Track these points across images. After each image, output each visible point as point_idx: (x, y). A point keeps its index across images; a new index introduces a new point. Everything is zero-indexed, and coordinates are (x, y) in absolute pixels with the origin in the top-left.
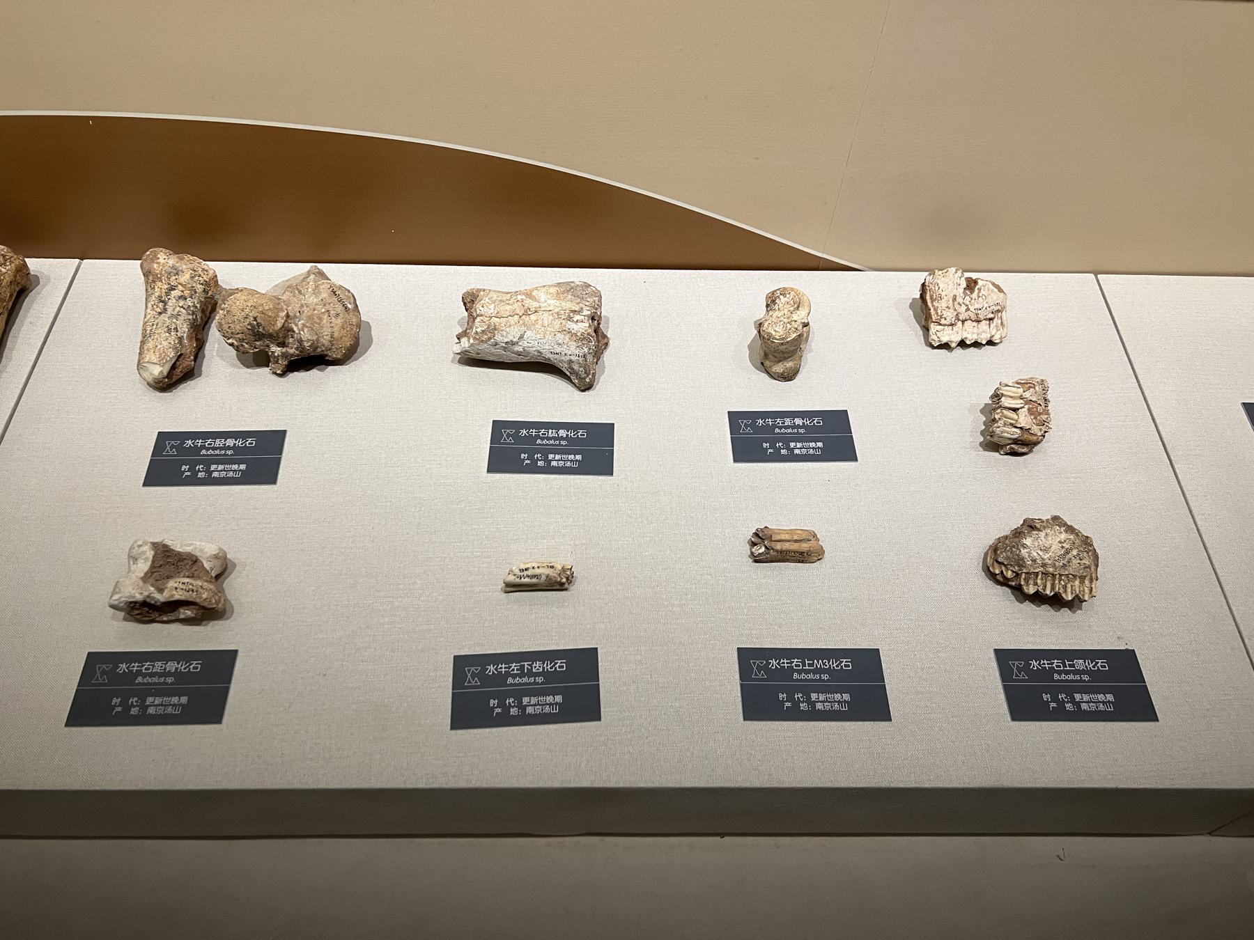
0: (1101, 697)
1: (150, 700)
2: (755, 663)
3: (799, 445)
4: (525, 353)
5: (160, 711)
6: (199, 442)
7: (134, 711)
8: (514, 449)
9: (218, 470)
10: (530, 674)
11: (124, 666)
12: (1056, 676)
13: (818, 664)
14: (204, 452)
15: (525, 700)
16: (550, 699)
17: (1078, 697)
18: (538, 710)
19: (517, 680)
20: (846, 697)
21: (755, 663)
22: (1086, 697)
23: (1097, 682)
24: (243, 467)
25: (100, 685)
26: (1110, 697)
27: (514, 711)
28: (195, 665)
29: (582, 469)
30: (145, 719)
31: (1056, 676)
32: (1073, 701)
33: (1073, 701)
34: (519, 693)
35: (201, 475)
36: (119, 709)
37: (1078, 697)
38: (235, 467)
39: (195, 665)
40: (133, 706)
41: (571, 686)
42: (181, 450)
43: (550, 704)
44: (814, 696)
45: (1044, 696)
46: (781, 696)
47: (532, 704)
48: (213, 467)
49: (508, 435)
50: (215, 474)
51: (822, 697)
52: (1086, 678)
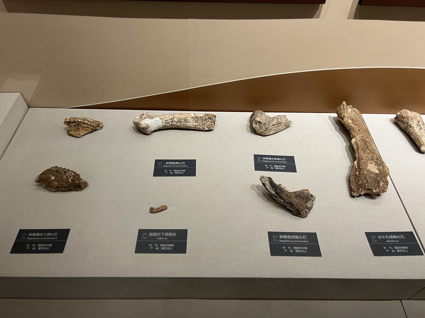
0: (403, 247)
1: (39, 245)
4: (187, 126)
7: (34, 249)
10: (164, 237)
11: (167, 233)
12: (387, 241)
15: (161, 245)
16: (170, 245)
17: (395, 248)
18: (165, 248)
19: (160, 239)
20: (306, 248)
23: (401, 243)
25: (23, 240)
26: (406, 248)
27: (157, 248)
28: (56, 234)
29: (185, 175)
31: (387, 241)
32: (394, 249)
34: (159, 243)
36: (29, 248)
37: (395, 248)
39: (175, 234)
40: (33, 247)
41: (177, 241)
43: (170, 247)
45: (283, 247)
46: (283, 247)
47: (163, 246)
51: (297, 248)
52: (397, 241)
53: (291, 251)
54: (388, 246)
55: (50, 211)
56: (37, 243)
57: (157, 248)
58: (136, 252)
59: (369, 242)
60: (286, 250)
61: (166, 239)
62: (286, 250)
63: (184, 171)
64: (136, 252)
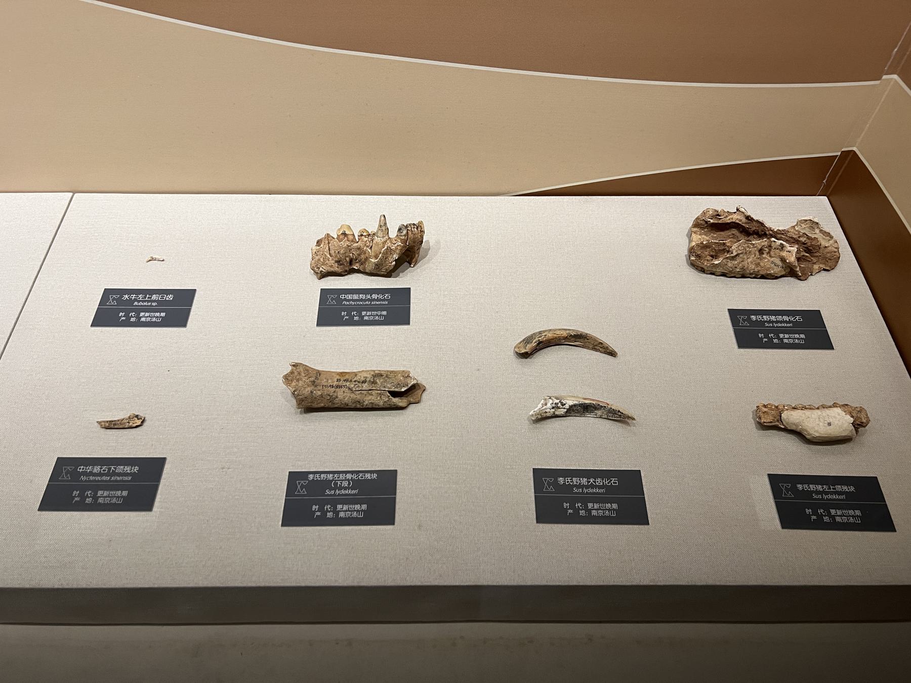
0: (851, 512)
1: (100, 493)
2: (784, 486)
3: (787, 336)
5: (107, 500)
6: (133, 297)
7: (89, 500)
8: (751, 330)
9: (145, 316)
13: (838, 488)
14: (136, 303)
16: (357, 507)
17: (833, 512)
20: (615, 506)
21: (547, 480)
22: (839, 512)
24: (163, 314)
26: (858, 513)
27: (330, 515)
30: (96, 507)
31: (575, 490)
32: (829, 515)
33: (829, 515)
35: (133, 320)
37: (833, 512)
38: (157, 314)
39: (375, 476)
41: (137, 483)
42: (120, 301)
43: (358, 511)
44: (590, 505)
45: (807, 511)
48: (142, 314)
49: (332, 299)
50: (143, 319)
53: (582, 513)
54: (815, 507)
55: (343, 445)
56: (96, 487)
57: (330, 515)
58: (319, 324)
59: (775, 497)
60: (570, 511)
61: (154, 304)
62: (570, 511)
63: (384, 313)
64: (319, 324)
